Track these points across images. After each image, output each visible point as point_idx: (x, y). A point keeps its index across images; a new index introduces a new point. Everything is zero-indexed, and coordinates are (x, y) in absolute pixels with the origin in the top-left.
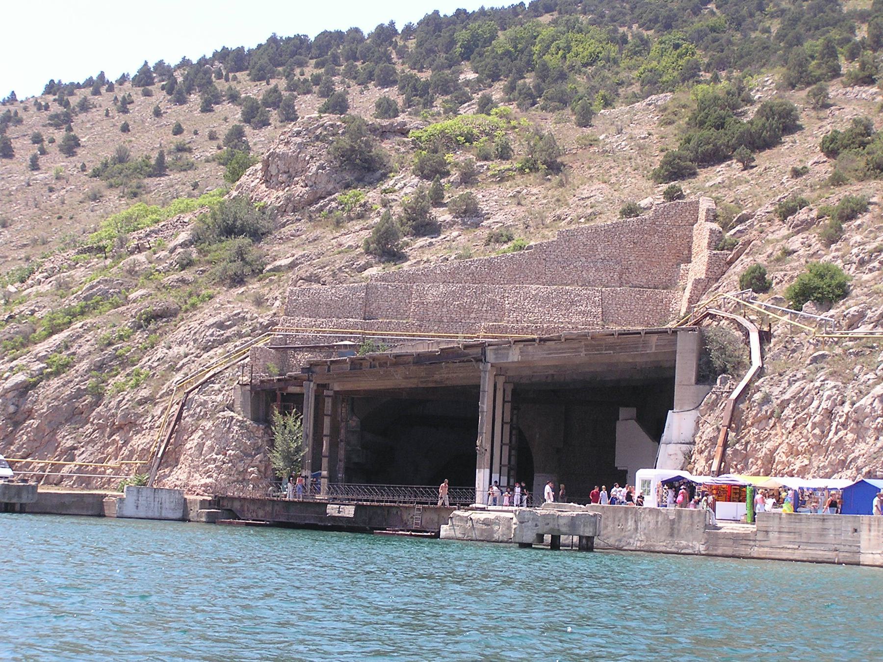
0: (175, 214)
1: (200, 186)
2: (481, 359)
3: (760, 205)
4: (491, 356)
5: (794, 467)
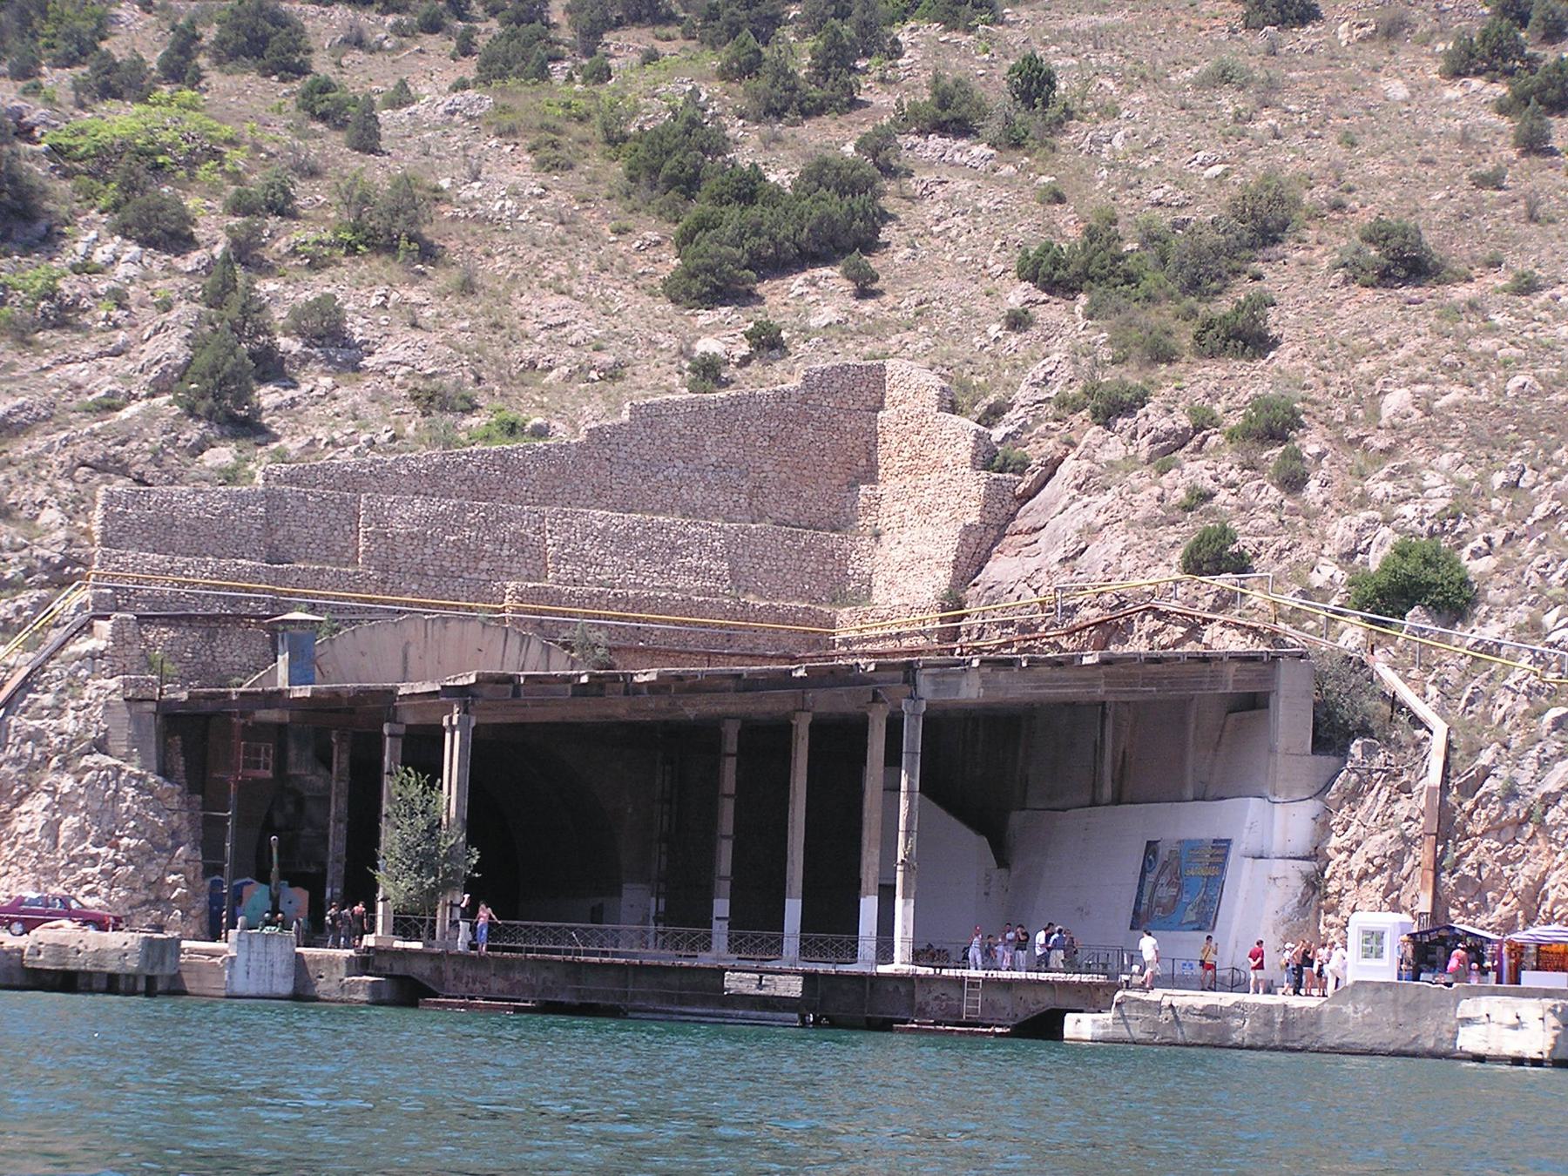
4: (925, 686)
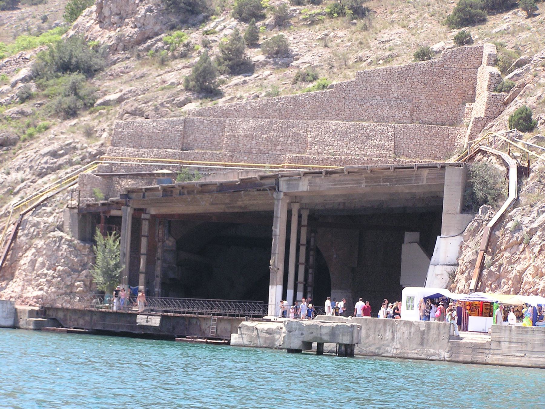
0: (19, 51)
1: (49, 20)
2: (275, 188)
3: (537, 51)
4: (283, 186)
5: (539, 287)
